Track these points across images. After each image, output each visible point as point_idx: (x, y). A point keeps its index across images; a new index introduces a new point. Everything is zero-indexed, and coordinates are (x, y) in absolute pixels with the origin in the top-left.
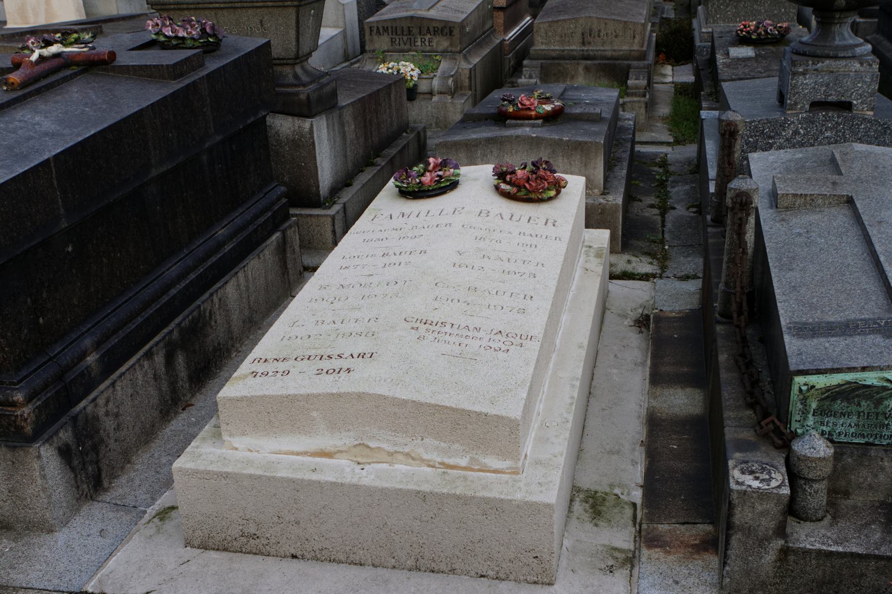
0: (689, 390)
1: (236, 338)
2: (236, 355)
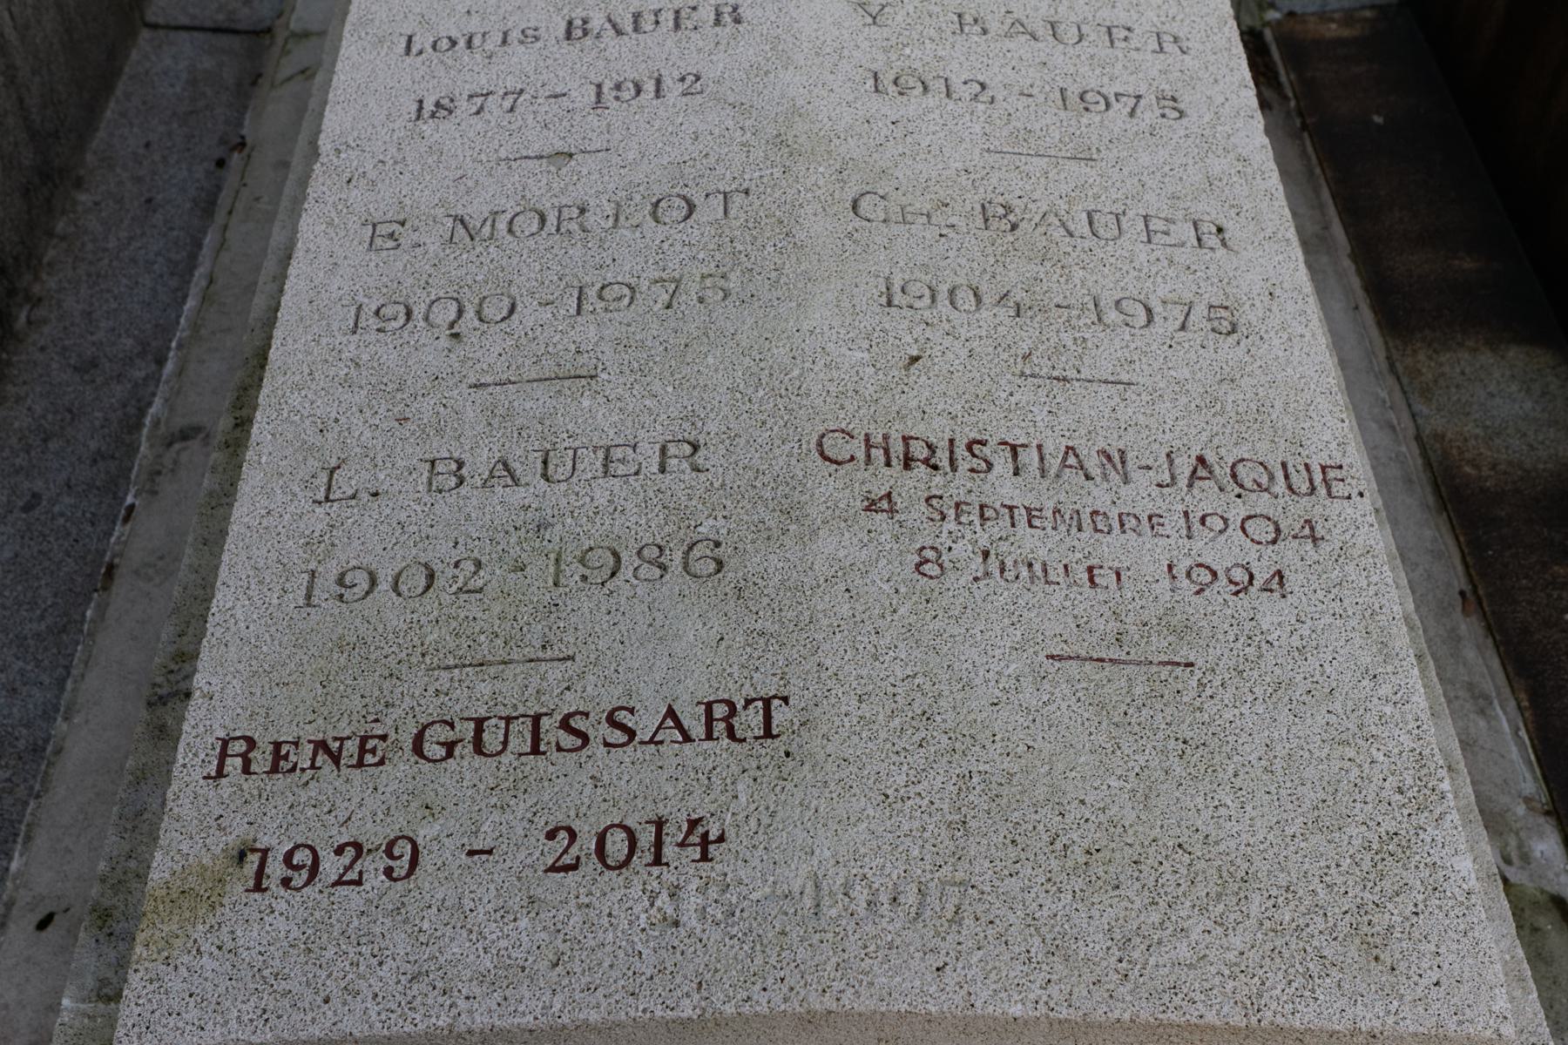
0: (1513, 352)
1: (16, 259)
2: (29, 322)
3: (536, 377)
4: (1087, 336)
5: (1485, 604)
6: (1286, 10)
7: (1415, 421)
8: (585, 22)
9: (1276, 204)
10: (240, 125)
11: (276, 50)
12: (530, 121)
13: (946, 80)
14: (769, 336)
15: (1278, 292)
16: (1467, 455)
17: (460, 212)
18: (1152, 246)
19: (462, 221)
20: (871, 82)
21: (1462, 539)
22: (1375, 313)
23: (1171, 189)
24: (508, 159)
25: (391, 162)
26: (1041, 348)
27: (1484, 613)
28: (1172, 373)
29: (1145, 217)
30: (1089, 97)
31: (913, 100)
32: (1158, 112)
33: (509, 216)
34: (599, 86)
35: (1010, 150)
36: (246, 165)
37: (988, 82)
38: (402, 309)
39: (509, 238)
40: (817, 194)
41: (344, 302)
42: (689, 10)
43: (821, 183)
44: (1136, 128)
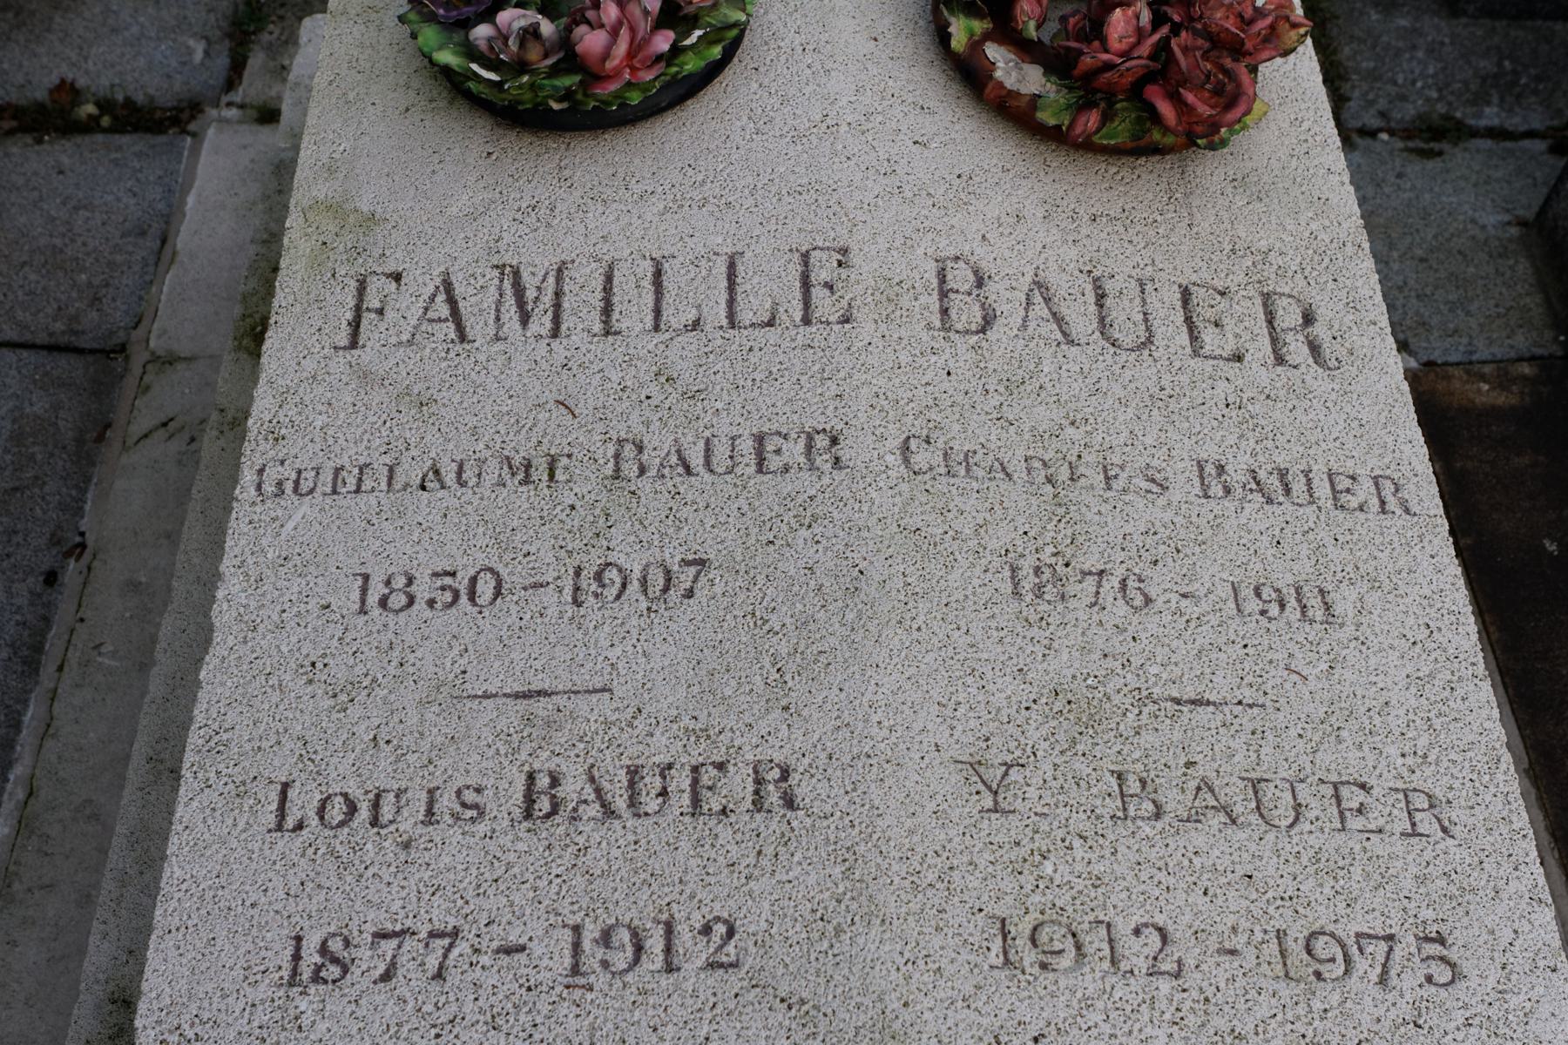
6: (1425, 359)
10: (79, 512)
11: (131, 382)
12: (469, 1007)
13: (1109, 925)
30: (1319, 944)
31: (1062, 984)
34: (577, 929)
37: (1170, 928)
42: (713, 772)
44: (1392, 1014)
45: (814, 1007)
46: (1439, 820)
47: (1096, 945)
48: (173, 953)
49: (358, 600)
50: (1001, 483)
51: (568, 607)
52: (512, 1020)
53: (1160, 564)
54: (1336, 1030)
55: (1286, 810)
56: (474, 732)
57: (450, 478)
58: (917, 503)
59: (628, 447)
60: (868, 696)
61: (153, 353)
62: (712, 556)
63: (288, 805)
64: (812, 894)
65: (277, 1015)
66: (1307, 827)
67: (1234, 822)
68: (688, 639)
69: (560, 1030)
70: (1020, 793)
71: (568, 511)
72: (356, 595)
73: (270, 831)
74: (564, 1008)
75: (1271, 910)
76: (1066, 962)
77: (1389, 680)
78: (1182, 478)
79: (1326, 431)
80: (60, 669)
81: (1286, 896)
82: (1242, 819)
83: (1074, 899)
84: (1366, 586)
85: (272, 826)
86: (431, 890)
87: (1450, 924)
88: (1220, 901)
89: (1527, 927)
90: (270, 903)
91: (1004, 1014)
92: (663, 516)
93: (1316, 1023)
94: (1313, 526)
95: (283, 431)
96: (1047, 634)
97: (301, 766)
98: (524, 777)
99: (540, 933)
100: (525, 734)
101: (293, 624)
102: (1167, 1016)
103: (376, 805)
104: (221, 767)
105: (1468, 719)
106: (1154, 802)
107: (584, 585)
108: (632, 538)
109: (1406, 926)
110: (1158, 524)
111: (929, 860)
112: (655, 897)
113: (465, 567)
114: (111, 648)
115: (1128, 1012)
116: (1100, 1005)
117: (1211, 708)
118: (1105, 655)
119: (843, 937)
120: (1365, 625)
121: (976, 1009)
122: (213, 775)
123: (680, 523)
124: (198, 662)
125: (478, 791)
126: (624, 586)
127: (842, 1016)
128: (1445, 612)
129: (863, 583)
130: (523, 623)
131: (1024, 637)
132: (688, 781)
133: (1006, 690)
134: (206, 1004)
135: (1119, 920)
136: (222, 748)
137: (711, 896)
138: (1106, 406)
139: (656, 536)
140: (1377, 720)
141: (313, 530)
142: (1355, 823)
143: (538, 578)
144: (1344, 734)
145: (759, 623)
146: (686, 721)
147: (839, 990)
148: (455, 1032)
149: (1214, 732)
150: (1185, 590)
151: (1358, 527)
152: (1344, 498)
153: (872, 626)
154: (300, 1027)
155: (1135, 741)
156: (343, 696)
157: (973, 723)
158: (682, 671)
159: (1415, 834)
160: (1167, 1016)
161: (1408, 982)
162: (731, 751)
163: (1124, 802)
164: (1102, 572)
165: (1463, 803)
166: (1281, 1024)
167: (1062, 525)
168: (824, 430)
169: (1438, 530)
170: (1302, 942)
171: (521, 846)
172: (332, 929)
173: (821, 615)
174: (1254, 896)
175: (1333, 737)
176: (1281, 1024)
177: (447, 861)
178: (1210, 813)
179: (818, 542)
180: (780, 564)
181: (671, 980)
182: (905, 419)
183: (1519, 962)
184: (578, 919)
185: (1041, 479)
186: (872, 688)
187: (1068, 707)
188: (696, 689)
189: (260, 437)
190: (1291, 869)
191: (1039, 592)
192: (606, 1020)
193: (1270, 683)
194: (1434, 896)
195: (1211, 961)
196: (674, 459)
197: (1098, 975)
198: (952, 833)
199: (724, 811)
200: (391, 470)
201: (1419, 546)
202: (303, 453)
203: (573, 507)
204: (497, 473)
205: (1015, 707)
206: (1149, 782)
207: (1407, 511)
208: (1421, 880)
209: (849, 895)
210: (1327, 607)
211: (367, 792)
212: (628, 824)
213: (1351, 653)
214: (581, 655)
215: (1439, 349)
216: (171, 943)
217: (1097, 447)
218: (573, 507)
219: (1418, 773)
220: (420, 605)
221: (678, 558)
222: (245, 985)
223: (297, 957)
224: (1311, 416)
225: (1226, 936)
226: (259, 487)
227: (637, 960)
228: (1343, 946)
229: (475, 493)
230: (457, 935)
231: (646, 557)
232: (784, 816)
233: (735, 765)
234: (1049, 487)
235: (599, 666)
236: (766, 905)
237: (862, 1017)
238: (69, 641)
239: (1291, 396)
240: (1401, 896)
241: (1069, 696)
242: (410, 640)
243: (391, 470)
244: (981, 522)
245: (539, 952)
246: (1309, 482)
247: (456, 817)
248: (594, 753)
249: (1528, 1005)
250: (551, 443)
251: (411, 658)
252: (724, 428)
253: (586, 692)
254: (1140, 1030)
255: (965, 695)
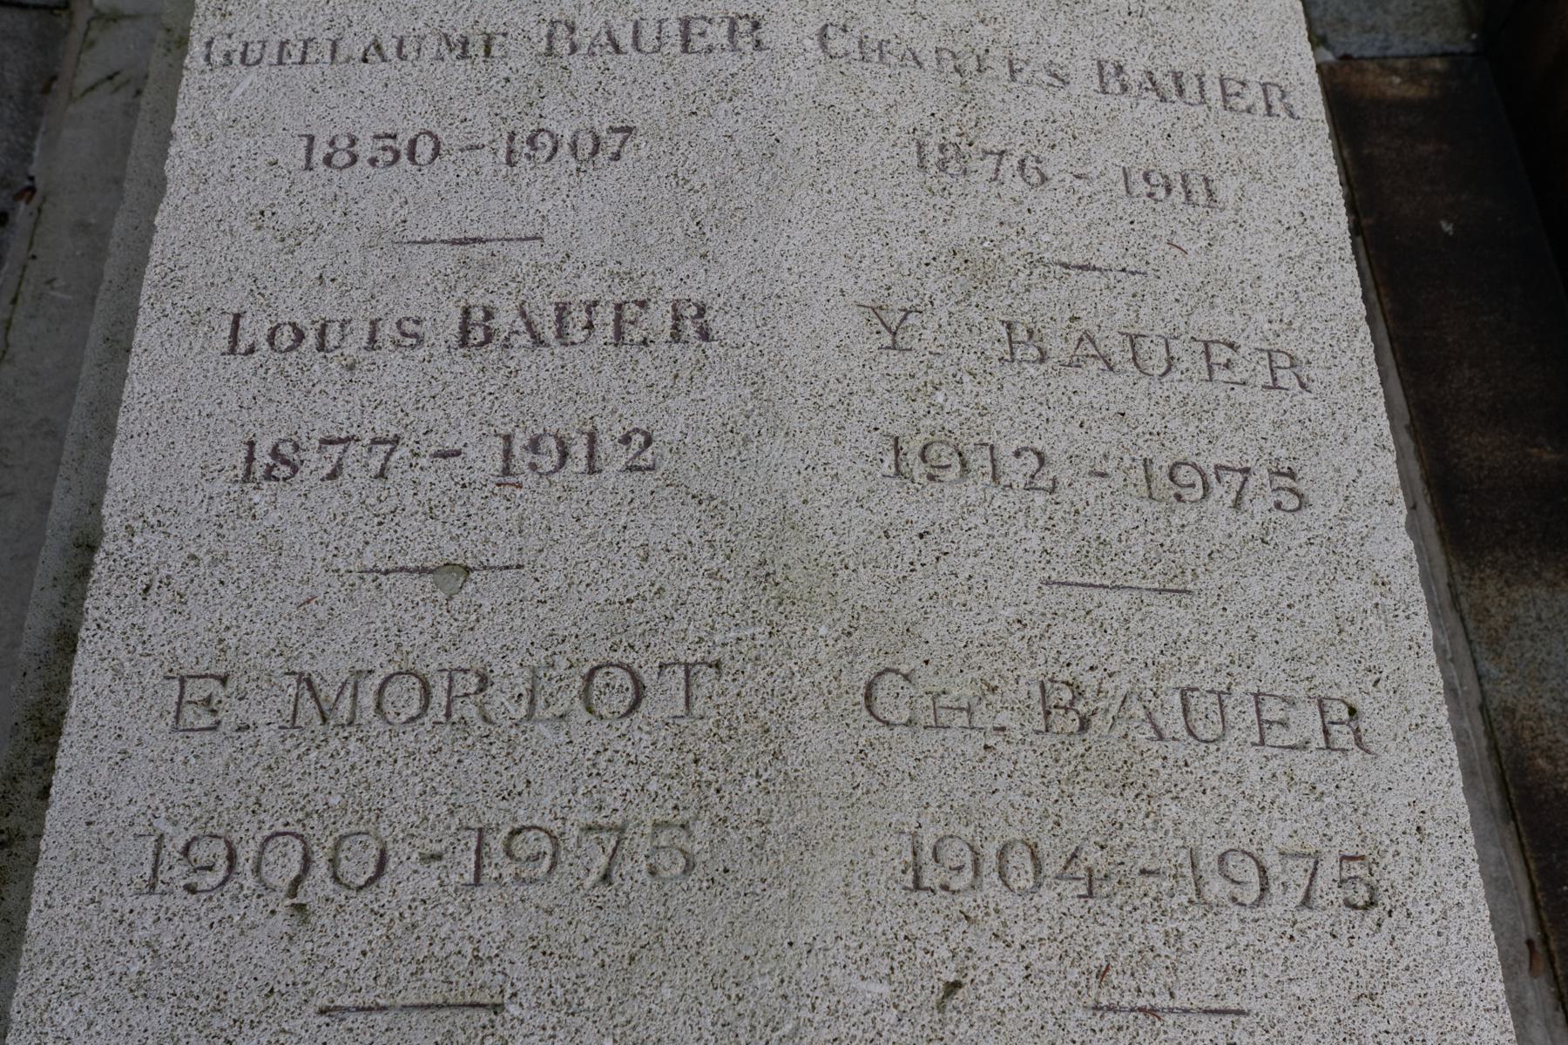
3: (416, 1002)
4: (1183, 927)
5: (1557, 965)
6: (1341, 53)
7: (1481, 685)
8: (489, 315)
9: (1424, 662)
10: (28, 158)
11: (76, 37)
12: (408, 500)
13: (992, 448)
14: (750, 952)
15: (1429, 826)
16: (1542, 742)
17: (306, 668)
18: (1268, 751)
19: (309, 682)
20: (889, 458)
21: (1533, 866)
22: (1438, 521)
23: (1289, 643)
24: (375, 570)
25: (208, 559)
26: (1123, 954)
27: (1556, 977)
28: (1295, 989)
29: (1256, 696)
30: (1181, 473)
31: (948, 491)
32: (1272, 499)
33: (378, 682)
34: (508, 438)
35: (1079, 580)
36: (36, 224)
37: (1048, 452)
38: (220, 849)
39: (378, 724)
40: (818, 678)
41: (137, 829)
42: (636, 308)
43: (822, 657)
44: (1243, 531)
45: (722, 502)
46: (1298, 377)
47: (980, 462)
48: (135, 454)
49: (303, 157)
50: (912, 70)
51: (502, 167)
52: (448, 511)
53: (1058, 148)
54: (1191, 541)
55: (1160, 361)
56: (413, 272)
57: (390, 52)
58: (832, 83)
59: (560, 29)
60: (781, 246)
61: (97, 11)
62: (638, 125)
63: (240, 332)
64: (723, 410)
65: (233, 506)
66: (1178, 376)
67: (1111, 369)
68: (615, 195)
69: (492, 519)
70: (917, 335)
71: (503, 83)
72: (302, 153)
73: (223, 354)
74: (495, 502)
75: (1140, 442)
76: (952, 474)
77: (1262, 259)
78: (1082, 75)
79: (1221, 41)
80: (14, 301)
81: (1155, 432)
82: (1118, 367)
83: (962, 424)
84: (1247, 176)
85: (226, 350)
86: (374, 404)
87: (1300, 462)
88: (1094, 432)
89: (1370, 468)
90: (225, 414)
91: (894, 513)
92: (593, 89)
93: (1174, 535)
94: (1202, 123)
95: (230, 8)
96: (949, 202)
97: (251, 299)
98: (460, 311)
99: (474, 440)
100: (461, 274)
101: (242, 177)
102: (1041, 523)
103: (322, 334)
104: (177, 299)
105: (1332, 294)
106: (1039, 349)
107: (517, 147)
108: (564, 108)
109: (1261, 461)
110: (1057, 113)
111: (831, 385)
112: (579, 412)
113: (405, 130)
114: (63, 283)
115: (1005, 518)
116: (980, 511)
117: (1097, 273)
118: (1002, 223)
119: (750, 446)
120: (1244, 210)
121: (868, 509)
122: (169, 306)
123: (608, 95)
124: (154, 211)
125: (417, 322)
126: (555, 149)
127: (747, 509)
128: (1319, 203)
129: (779, 150)
130: (459, 180)
131: (927, 204)
132: (612, 317)
133: (907, 247)
134: (167, 496)
135: (1002, 443)
136: (177, 283)
137: (631, 411)
138: (1015, 8)
139: (586, 107)
140: (1249, 291)
141: (260, 96)
142: (1221, 375)
143: (474, 141)
144: (1218, 301)
145: (681, 183)
146: (611, 265)
147: (745, 489)
148: (396, 520)
149: (1098, 293)
150: (1080, 171)
151: (1245, 126)
152: (1233, 101)
153: (786, 187)
154: (254, 516)
155: (1025, 297)
156: (290, 240)
157: (876, 274)
158: (608, 223)
159: (1275, 387)
160: (1041, 523)
161: (1260, 507)
162: (653, 291)
163: (1011, 348)
164: (1003, 152)
165: (1321, 364)
166: (1143, 535)
167: (968, 109)
168: (747, 16)
169: (1318, 133)
170: (1165, 470)
171: (457, 369)
172: (283, 436)
173: (739, 177)
174: (1126, 430)
175: (1207, 304)
176: (1143, 535)
177: (388, 380)
178: (1090, 360)
179: (738, 114)
180: (702, 132)
181: (593, 480)
182: (823, 9)
183: (1360, 494)
184: (509, 429)
185: (950, 68)
186: (784, 239)
187: (964, 265)
188: (621, 238)
189: (208, 13)
190: (1160, 410)
191: (943, 165)
192: (534, 512)
193: (1153, 255)
194: (1288, 439)
195: (1083, 481)
196: (604, 39)
197: (980, 487)
198: (853, 364)
199: (644, 342)
200: (334, 44)
201: (1300, 145)
202: (248, 27)
203: (507, 80)
204: (435, 48)
205: (916, 263)
206: (1036, 331)
207: (1292, 115)
208: (1278, 425)
209: (757, 411)
210: (1210, 193)
211: (313, 322)
212: (556, 351)
213: (1229, 233)
214: (514, 209)
215: (1355, 44)
216: (134, 446)
217: (1004, 43)
218: (507, 80)
219: (1283, 337)
220: (363, 163)
221: (606, 126)
222: (203, 481)
223: (250, 459)
224: (1207, 27)
225: (1098, 461)
226: (208, 58)
227: (562, 463)
228: (1203, 475)
229: (414, 66)
230: (397, 442)
231: (575, 125)
232: (700, 346)
233: (656, 303)
234: (957, 76)
235: (531, 218)
236: (681, 419)
237: (765, 511)
238: (22, 276)
239: (1191, 8)
240: (1259, 436)
241: (966, 256)
242: (353, 193)
243: (334, 44)
244: (892, 103)
245: (474, 456)
246: (1201, 84)
247: (397, 344)
248: (525, 291)
249: (1365, 531)
250: (487, 22)
251: (355, 208)
252: (652, 13)
253: (518, 239)
254: (1016, 533)
255: (870, 250)
